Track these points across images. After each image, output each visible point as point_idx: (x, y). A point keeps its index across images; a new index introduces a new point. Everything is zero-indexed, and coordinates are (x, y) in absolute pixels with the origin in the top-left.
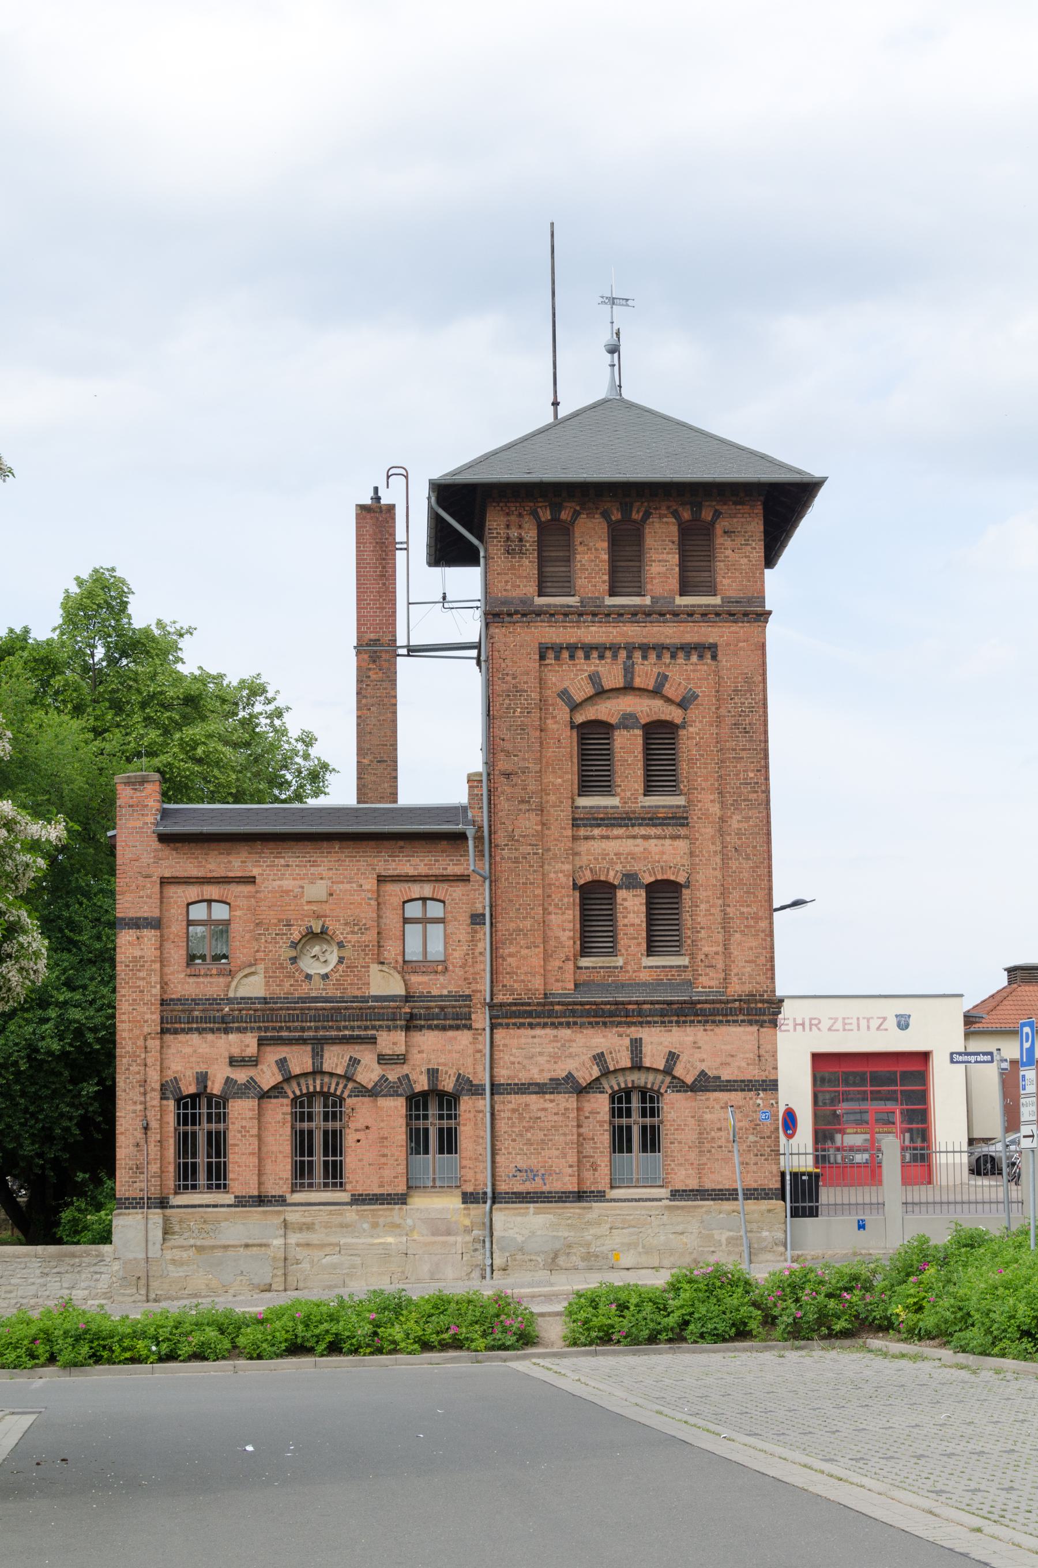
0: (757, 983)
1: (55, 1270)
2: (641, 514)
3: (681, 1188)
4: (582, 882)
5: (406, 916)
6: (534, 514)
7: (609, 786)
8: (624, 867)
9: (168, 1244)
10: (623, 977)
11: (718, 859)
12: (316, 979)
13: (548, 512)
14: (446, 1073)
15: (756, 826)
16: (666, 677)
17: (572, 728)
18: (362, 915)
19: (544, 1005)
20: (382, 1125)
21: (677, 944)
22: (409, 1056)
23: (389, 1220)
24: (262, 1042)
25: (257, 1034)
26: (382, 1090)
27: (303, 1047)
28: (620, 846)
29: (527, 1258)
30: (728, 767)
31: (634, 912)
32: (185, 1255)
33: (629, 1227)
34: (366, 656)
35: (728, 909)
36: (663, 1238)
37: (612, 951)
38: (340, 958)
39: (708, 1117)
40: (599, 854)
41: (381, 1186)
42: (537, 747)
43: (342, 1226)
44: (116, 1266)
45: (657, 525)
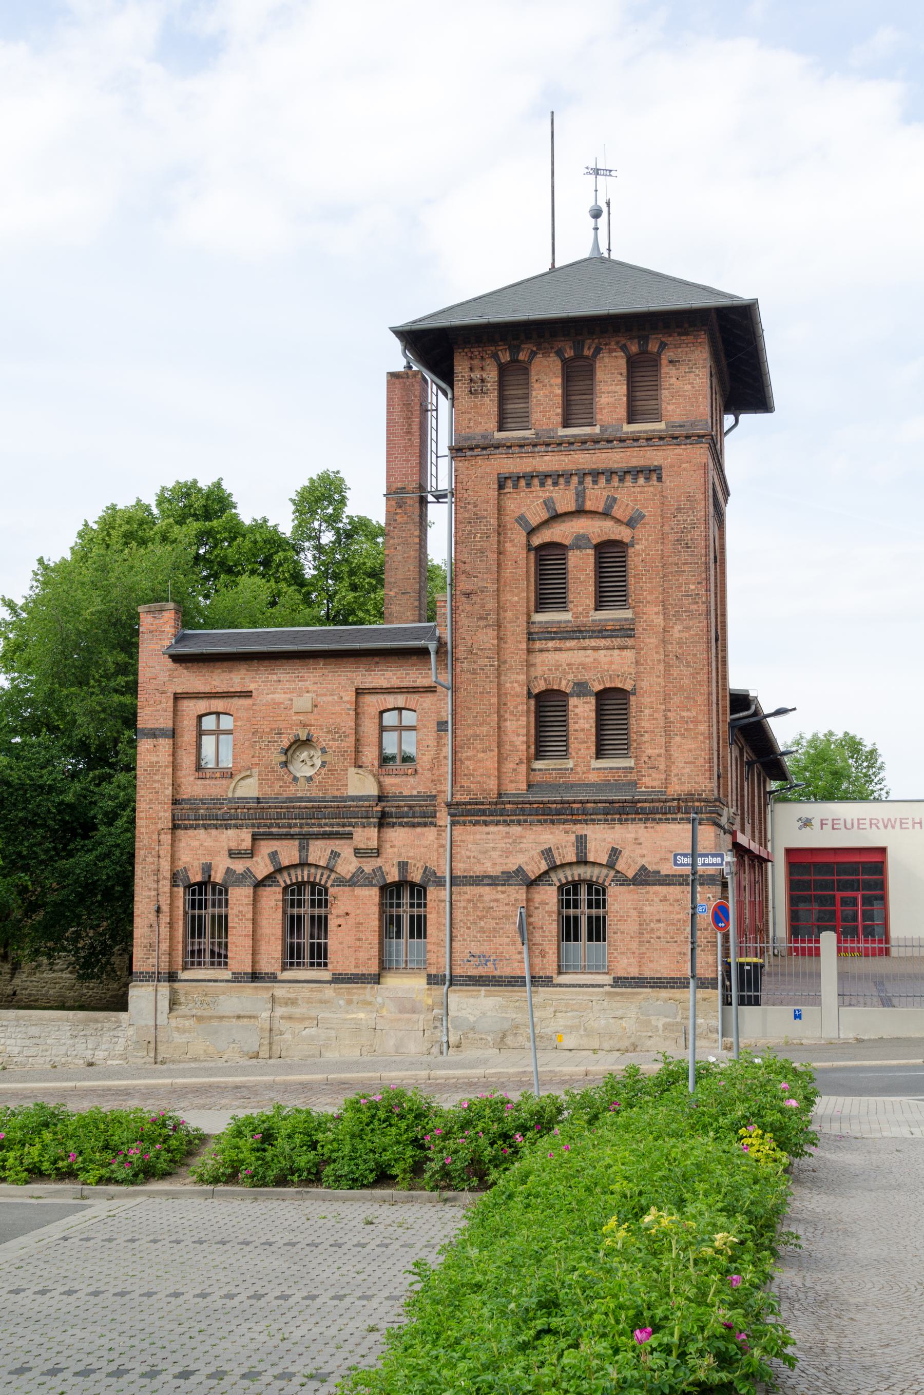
0: (695, 783)
1: (82, 1033)
2: (592, 350)
3: (623, 975)
4: (537, 691)
5: (385, 724)
6: (495, 356)
7: (564, 603)
8: (575, 676)
9: (174, 1014)
10: (573, 778)
11: (661, 667)
12: (302, 781)
13: (508, 354)
14: (415, 866)
15: (696, 635)
16: (615, 500)
17: (529, 550)
18: (342, 724)
19: (496, 804)
20: (358, 912)
21: (626, 747)
22: (382, 850)
23: (362, 997)
24: (255, 838)
25: (251, 830)
26: (359, 881)
27: (292, 842)
28: (572, 657)
29: (478, 1036)
30: (671, 580)
31: (584, 718)
32: (187, 1023)
33: (572, 1010)
34: (393, 503)
35: (669, 713)
36: (603, 1022)
37: (565, 754)
38: (323, 762)
39: (647, 909)
40: (552, 665)
41: (357, 967)
42: (494, 568)
43: (322, 1002)
44: (131, 1031)
45: (606, 360)
